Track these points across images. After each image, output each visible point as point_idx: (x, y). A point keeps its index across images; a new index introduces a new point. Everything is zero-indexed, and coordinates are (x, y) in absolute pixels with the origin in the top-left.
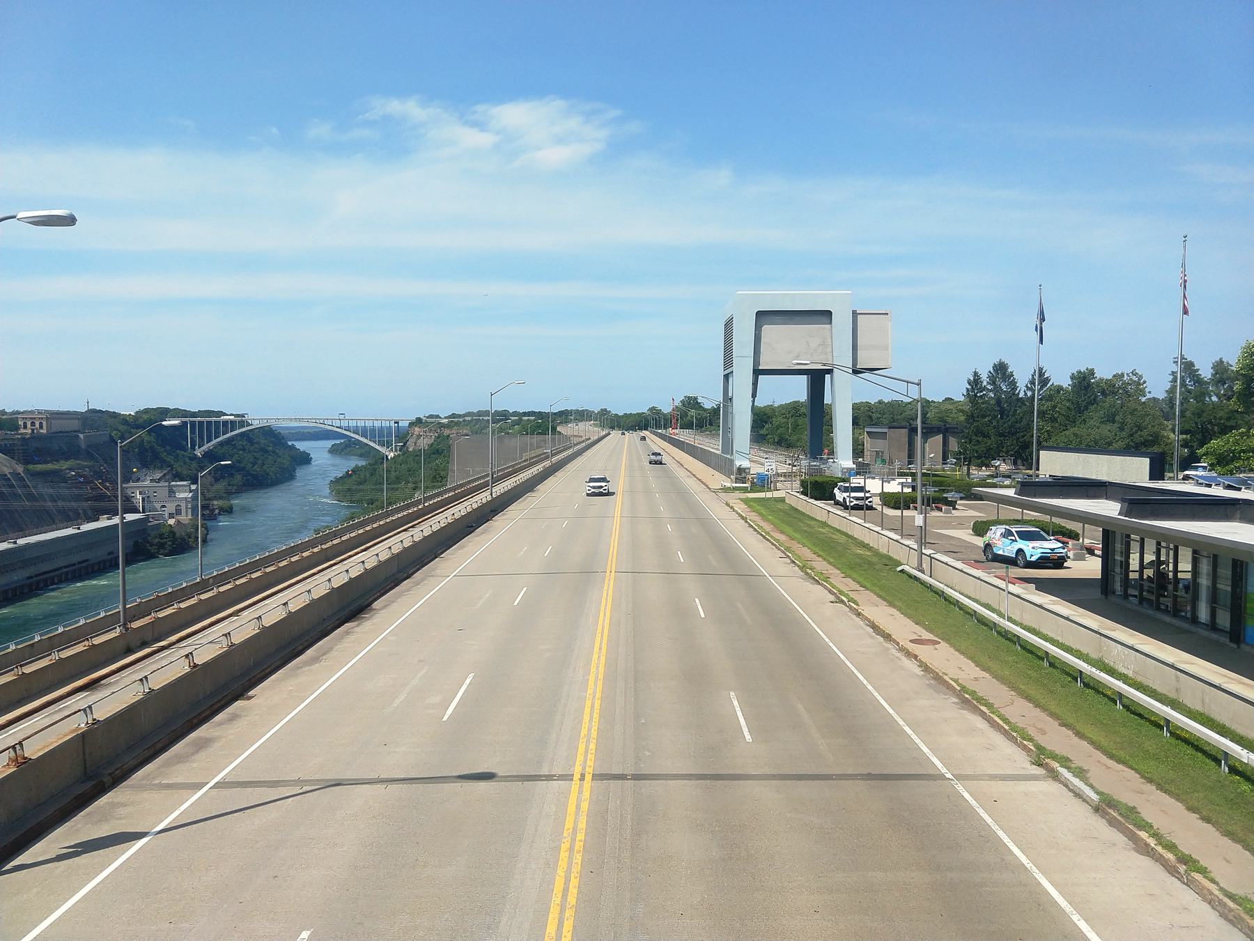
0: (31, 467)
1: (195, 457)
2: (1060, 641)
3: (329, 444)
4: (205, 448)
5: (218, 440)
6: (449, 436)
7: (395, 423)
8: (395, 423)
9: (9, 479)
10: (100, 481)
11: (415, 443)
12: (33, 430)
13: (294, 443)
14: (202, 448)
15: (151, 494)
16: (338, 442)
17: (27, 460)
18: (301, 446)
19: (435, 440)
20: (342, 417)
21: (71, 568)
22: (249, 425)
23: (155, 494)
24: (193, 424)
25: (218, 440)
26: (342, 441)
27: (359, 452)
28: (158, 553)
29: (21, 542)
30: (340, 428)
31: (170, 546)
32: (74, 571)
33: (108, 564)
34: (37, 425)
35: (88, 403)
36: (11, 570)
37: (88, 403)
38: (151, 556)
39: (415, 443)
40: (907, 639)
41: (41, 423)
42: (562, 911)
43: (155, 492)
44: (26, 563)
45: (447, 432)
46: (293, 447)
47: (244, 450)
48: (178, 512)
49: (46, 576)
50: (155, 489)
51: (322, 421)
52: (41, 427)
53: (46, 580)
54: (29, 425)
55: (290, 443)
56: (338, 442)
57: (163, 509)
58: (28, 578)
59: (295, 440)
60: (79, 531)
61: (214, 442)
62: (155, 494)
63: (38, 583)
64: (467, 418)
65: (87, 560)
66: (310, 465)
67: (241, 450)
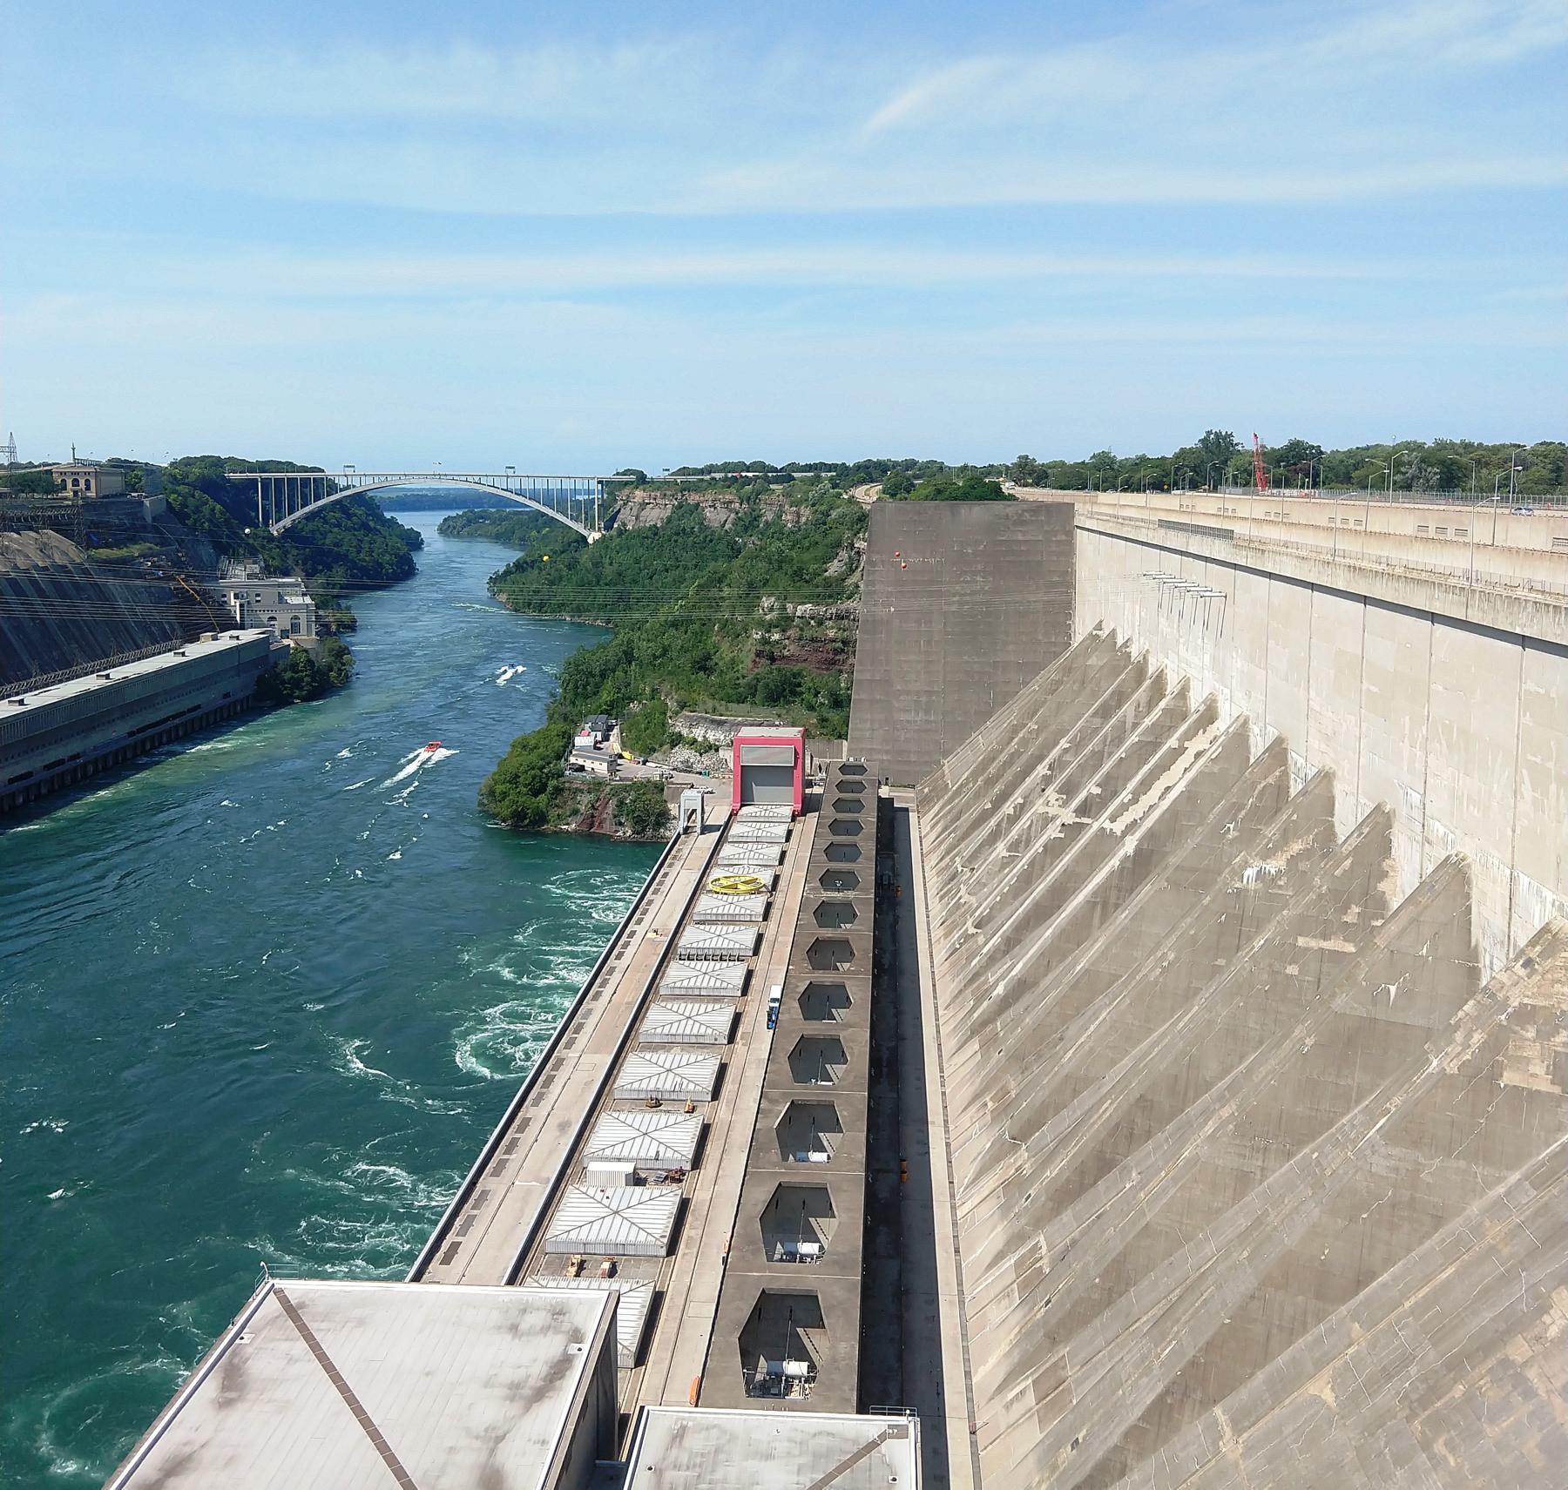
0: (92, 552)
1: (271, 538)
2: (1032, 1435)
3: (439, 517)
4: (287, 522)
5: (307, 509)
6: (698, 504)
7: (599, 482)
8: (599, 482)
9: (70, 572)
10: (183, 576)
11: (637, 518)
12: (76, 493)
13: (394, 514)
14: (281, 524)
15: (253, 598)
16: (453, 513)
17: (88, 543)
18: (407, 520)
19: (673, 512)
20: (349, 471)
21: (183, 719)
22: (333, 488)
23: (258, 598)
24: (266, 482)
25: (307, 509)
26: (461, 513)
27: (494, 530)
28: (291, 696)
29: (118, 674)
30: (506, 490)
31: (308, 684)
32: (185, 724)
33: (212, 720)
34: (82, 485)
35: (74, 449)
36: (109, 722)
37: (74, 449)
38: (283, 702)
39: (637, 518)
40: (1522, 654)
41: (87, 481)
42: (1101, 1115)
43: (258, 595)
44: (128, 710)
45: (693, 498)
46: (393, 521)
47: (338, 525)
48: (295, 628)
49: (158, 729)
50: (259, 591)
51: (477, 479)
52: (88, 488)
53: (152, 738)
54: (69, 485)
55: (388, 515)
56: (453, 513)
57: (272, 623)
58: (131, 734)
59: (395, 510)
60: (184, 659)
61: (298, 514)
62: (258, 598)
63: (143, 742)
64: (718, 476)
65: (199, 707)
66: (421, 553)
67: (335, 526)
